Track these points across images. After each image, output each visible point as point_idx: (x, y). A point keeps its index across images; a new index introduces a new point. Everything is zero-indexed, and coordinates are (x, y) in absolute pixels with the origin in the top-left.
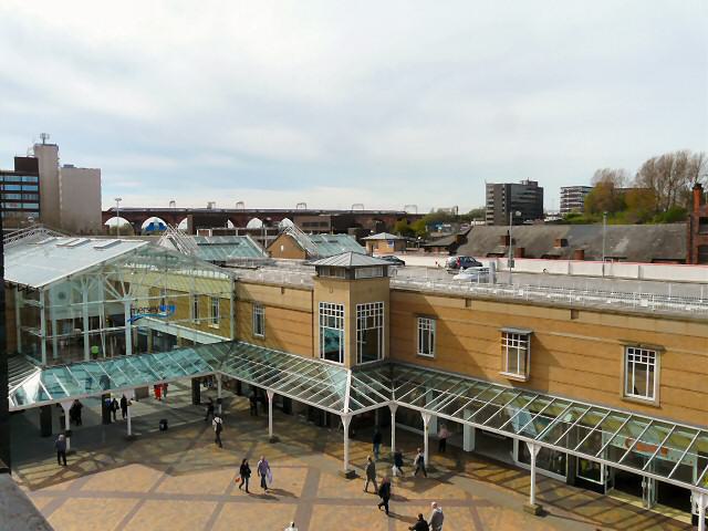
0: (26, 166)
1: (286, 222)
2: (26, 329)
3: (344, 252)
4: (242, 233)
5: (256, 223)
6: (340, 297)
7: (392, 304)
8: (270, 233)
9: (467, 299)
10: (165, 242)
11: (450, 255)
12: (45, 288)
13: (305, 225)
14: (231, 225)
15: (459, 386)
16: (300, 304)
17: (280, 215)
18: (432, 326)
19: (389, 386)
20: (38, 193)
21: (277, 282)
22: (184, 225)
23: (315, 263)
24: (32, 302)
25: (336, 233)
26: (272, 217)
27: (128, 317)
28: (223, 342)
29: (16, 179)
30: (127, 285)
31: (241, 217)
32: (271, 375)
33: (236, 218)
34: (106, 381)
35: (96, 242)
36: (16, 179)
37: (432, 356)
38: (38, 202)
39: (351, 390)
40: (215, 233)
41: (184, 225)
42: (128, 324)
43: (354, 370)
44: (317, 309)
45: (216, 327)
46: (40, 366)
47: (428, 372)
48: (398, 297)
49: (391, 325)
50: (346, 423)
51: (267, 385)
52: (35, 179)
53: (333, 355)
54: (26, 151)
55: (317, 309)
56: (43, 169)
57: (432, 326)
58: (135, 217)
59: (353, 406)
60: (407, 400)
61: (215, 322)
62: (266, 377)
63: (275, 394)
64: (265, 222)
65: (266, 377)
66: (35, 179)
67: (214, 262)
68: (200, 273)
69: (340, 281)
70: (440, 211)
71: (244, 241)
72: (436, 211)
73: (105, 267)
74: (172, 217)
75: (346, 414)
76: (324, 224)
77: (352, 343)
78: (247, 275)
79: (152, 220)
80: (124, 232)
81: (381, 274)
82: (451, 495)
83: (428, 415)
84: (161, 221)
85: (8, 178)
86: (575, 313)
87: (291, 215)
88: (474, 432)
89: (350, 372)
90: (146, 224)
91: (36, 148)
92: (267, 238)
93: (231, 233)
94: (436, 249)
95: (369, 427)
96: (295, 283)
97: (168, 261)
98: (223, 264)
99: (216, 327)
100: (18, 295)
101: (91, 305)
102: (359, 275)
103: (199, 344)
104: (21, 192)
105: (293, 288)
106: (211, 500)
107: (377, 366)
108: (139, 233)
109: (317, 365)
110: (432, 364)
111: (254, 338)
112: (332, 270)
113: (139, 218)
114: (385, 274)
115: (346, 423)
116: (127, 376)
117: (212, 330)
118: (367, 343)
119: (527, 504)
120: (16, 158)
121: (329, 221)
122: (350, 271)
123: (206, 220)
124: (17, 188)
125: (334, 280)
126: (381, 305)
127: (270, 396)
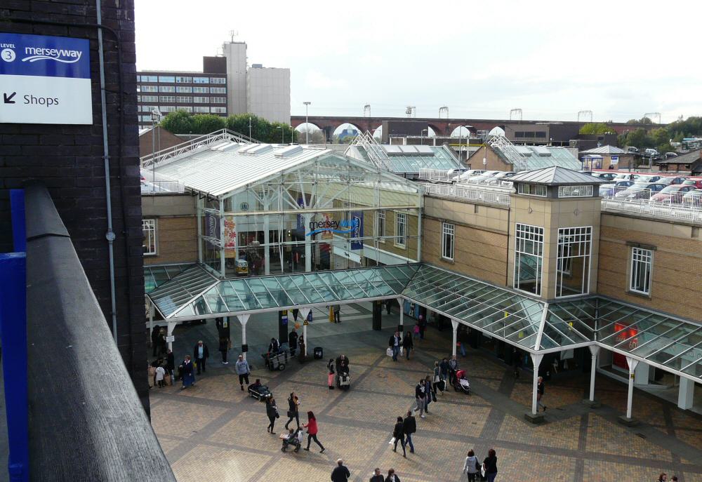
0: (215, 66)
1: (497, 131)
2: (206, 238)
3: (558, 165)
4: (439, 142)
5: (461, 132)
6: (539, 215)
7: (602, 229)
8: (473, 142)
9: (693, 227)
10: (352, 152)
11: (693, 174)
12: (225, 197)
13: (518, 134)
14: (431, 133)
15: (676, 330)
16: (495, 225)
17: (490, 124)
18: (650, 260)
19: (591, 323)
20: (225, 95)
21: (469, 198)
22: (378, 132)
23: (513, 178)
24: (212, 211)
25: (554, 144)
26: (478, 127)
27: (308, 230)
28: (408, 264)
29: (206, 80)
30: (308, 197)
31: (443, 126)
32: (458, 303)
33: (436, 125)
34: (283, 298)
35: (278, 149)
36: (206, 80)
37: (647, 294)
38: (225, 105)
39: (546, 324)
40: (410, 142)
41: (378, 132)
42: (308, 238)
43: (553, 304)
44: (513, 231)
45: (402, 246)
46: (220, 278)
47: (641, 312)
48: (612, 221)
49: (600, 254)
50: (536, 362)
51: (453, 313)
52: (223, 81)
53: (530, 287)
54: (217, 52)
55: (513, 231)
56: (231, 70)
57: (650, 260)
58: (327, 125)
59: (544, 343)
60: (613, 342)
61: (401, 242)
62: (453, 305)
63: (461, 325)
64: (472, 130)
65: (453, 305)
66: (223, 81)
67: (405, 175)
68: (385, 185)
69: (544, 199)
70: (691, 119)
71: (441, 151)
72: (685, 119)
73: (286, 177)
74: (366, 124)
75: (536, 351)
76: (541, 135)
77: (551, 272)
78: (438, 190)
79: (345, 126)
80: (314, 140)
81: (589, 192)
82: (655, 455)
83: (638, 361)
84: (354, 128)
85: (197, 80)
86: (696, 230)
87: (502, 124)
88: (688, 382)
89: (546, 305)
90: (338, 131)
91: (225, 46)
92: (469, 149)
93: (428, 142)
94: (676, 166)
95: (565, 373)
96: (489, 201)
97: (353, 172)
98: (415, 178)
99: (402, 246)
100: (200, 203)
101: (272, 218)
102: (562, 193)
103: (381, 265)
104: (158, 94)
105: (489, 206)
106: (384, 429)
107: (581, 301)
108: (329, 139)
109: (509, 294)
110: (647, 303)
111: (442, 260)
112: (533, 186)
113: (330, 124)
114: (596, 194)
115: (536, 362)
116: (309, 293)
117: (398, 251)
118: (571, 271)
119: (529, 414)
120: (288, 70)
121: (547, 130)
122: (553, 188)
123: (405, 129)
124: (155, 89)
125: (534, 198)
126: (589, 230)
127: (455, 326)
